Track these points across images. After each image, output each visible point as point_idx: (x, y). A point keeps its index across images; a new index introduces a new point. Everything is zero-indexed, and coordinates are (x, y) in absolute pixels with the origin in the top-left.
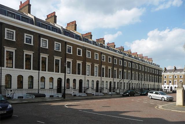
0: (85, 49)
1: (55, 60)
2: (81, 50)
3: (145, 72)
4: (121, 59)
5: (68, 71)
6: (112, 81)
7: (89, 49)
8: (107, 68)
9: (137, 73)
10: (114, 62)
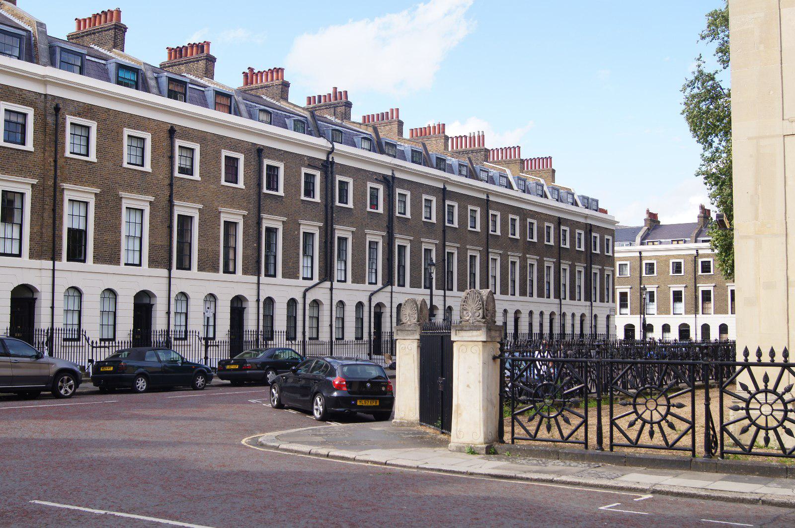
0: (57, 109)
1: (528, 265)
2: (30, 112)
3: (487, 241)
4: (312, 163)
5: (131, 253)
6: (556, 310)
7: (88, 111)
8: (209, 218)
9: (598, 272)
10: (259, 185)
